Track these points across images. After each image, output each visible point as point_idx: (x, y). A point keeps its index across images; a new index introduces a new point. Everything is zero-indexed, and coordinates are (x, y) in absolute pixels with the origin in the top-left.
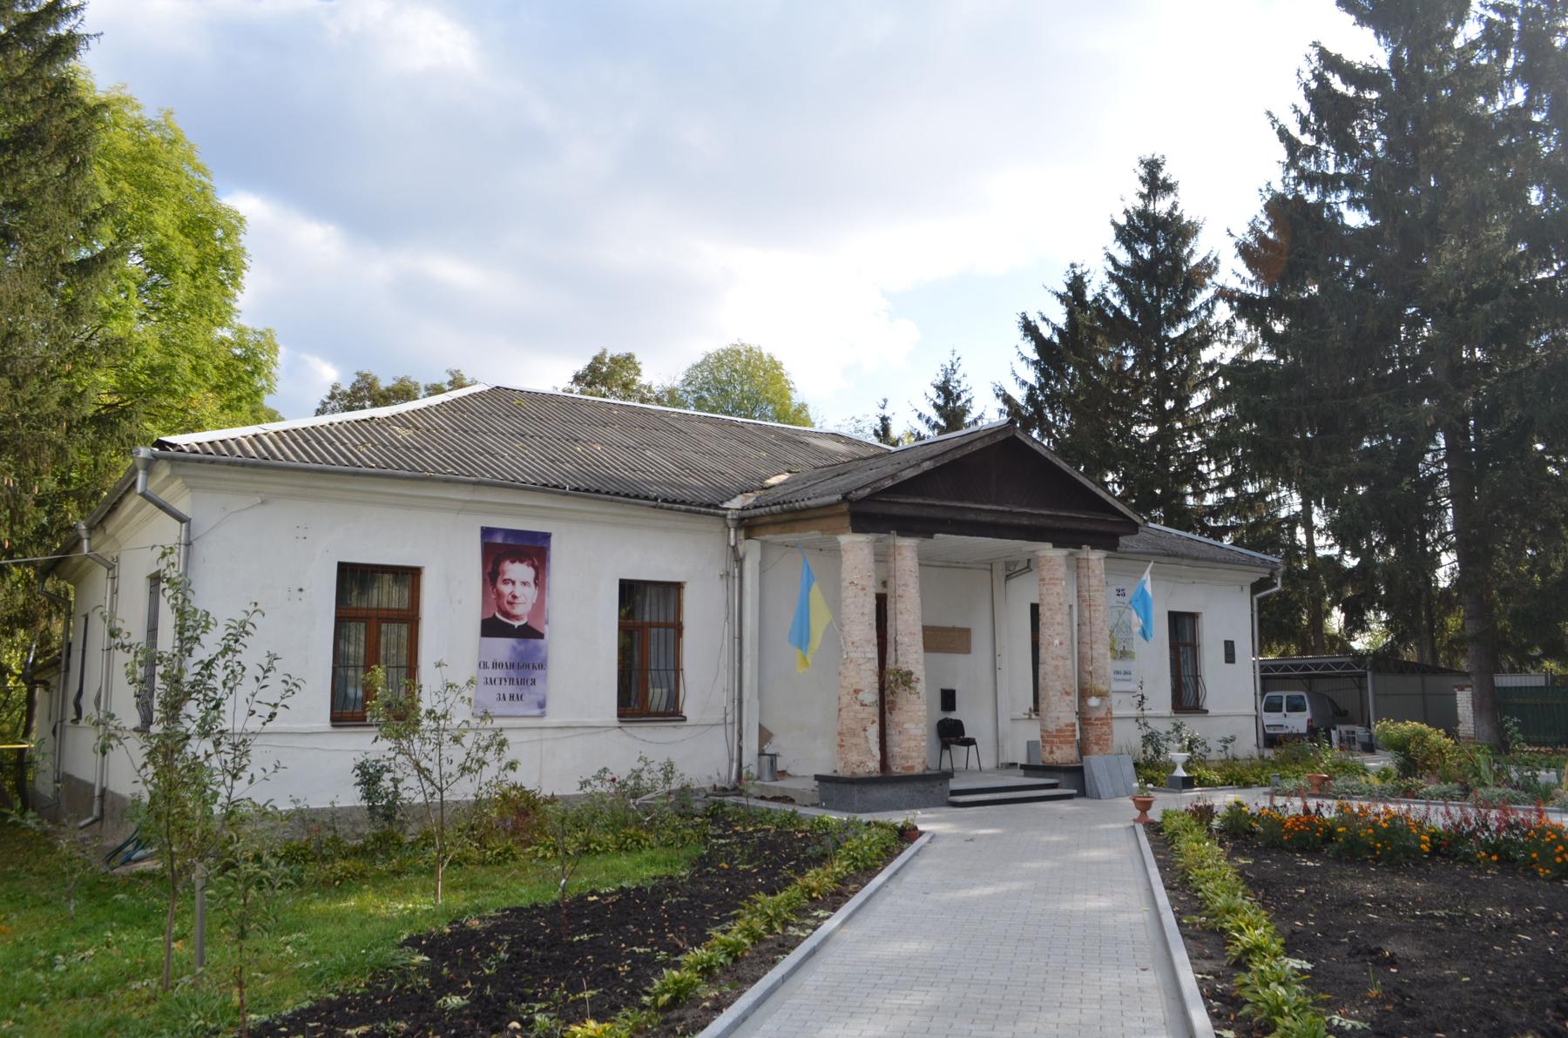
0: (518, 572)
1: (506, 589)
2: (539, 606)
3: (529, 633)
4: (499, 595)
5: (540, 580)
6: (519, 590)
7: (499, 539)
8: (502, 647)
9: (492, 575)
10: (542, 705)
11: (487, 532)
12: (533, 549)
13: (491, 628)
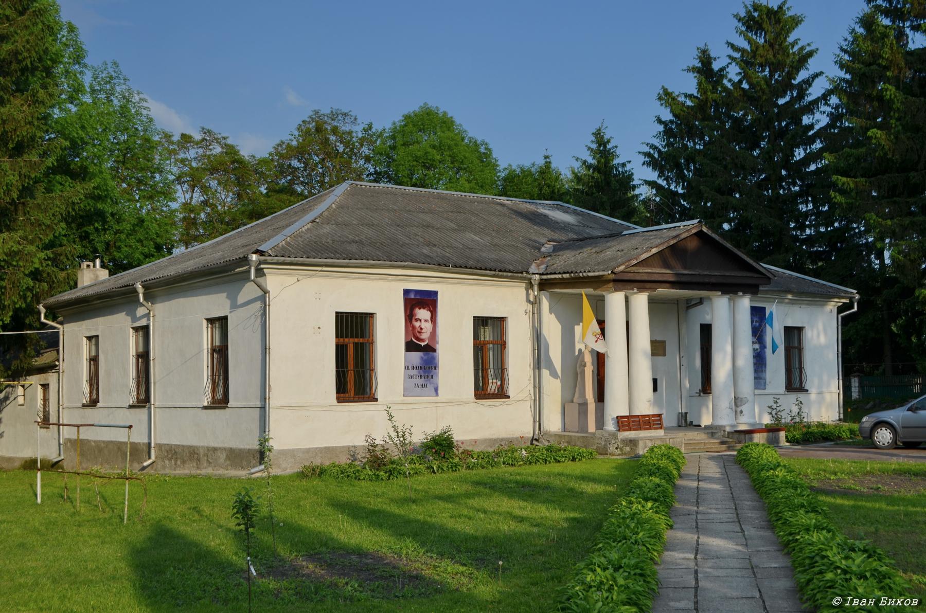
0: (423, 314)
1: (417, 324)
2: (434, 333)
3: (430, 349)
4: (414, 328)
5: (434, 319)
6: (423, 325)
7: (412, 296)
8: (416, 357)
9: (410, 317)
10: (436, 390)
11: (406, 292)
12: (427, 300)
13: (411, 347)
